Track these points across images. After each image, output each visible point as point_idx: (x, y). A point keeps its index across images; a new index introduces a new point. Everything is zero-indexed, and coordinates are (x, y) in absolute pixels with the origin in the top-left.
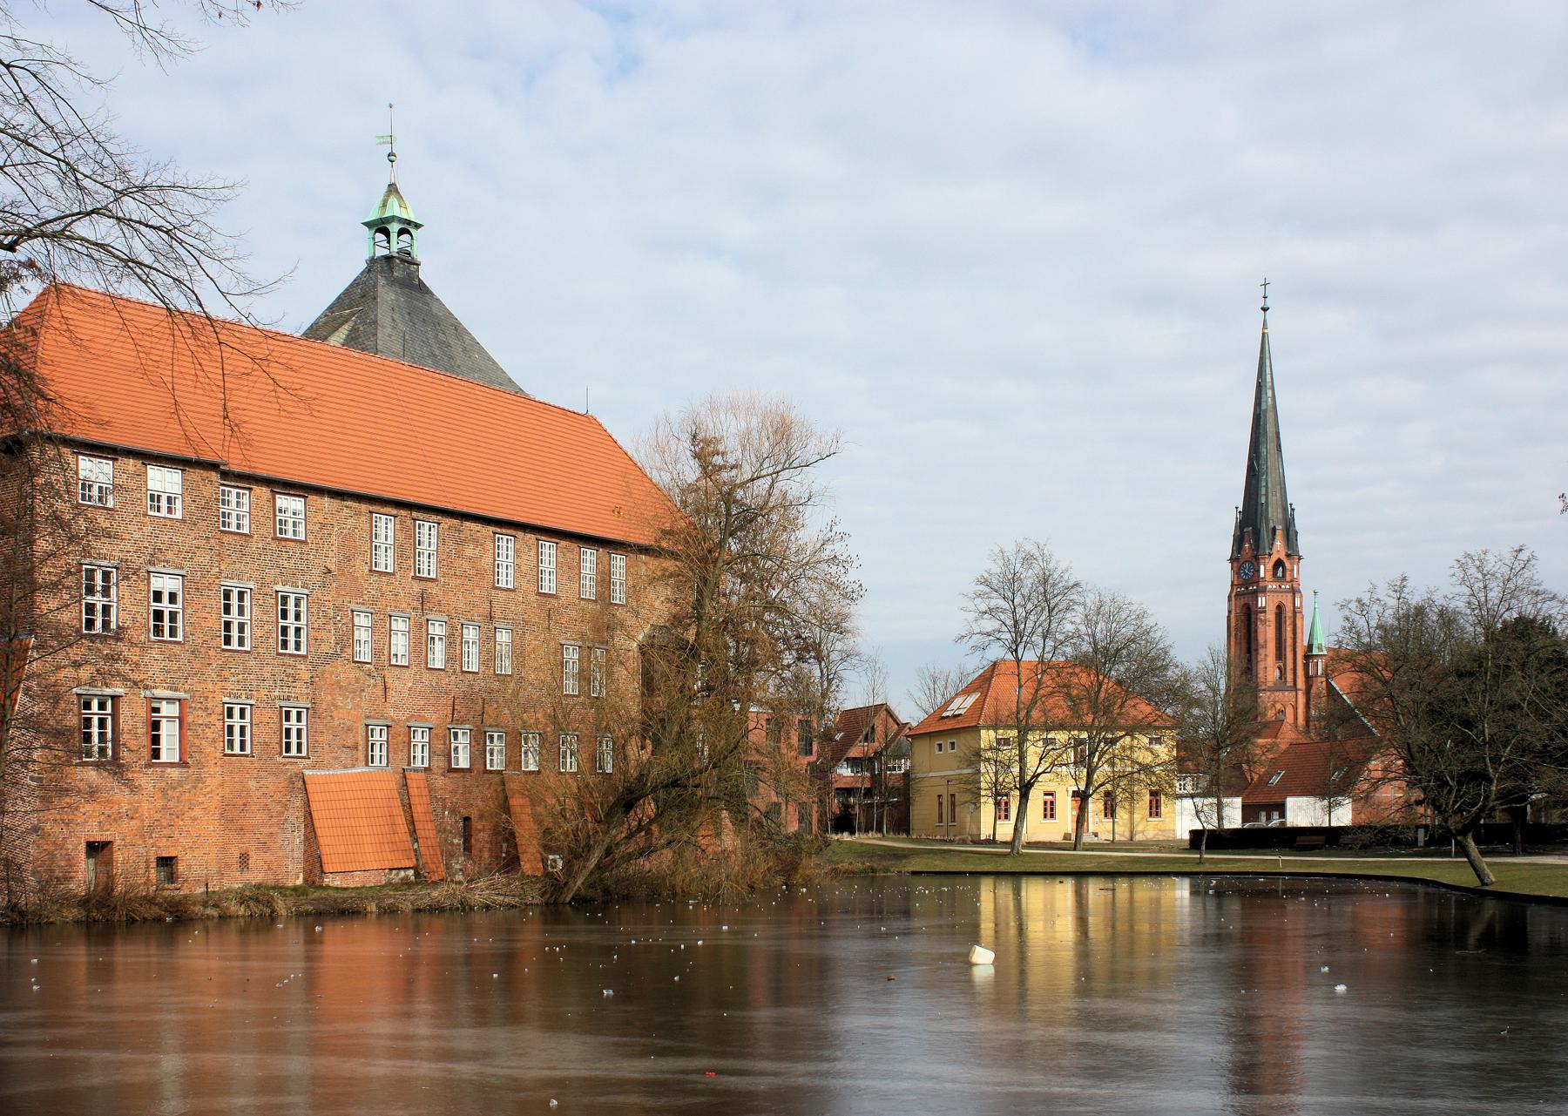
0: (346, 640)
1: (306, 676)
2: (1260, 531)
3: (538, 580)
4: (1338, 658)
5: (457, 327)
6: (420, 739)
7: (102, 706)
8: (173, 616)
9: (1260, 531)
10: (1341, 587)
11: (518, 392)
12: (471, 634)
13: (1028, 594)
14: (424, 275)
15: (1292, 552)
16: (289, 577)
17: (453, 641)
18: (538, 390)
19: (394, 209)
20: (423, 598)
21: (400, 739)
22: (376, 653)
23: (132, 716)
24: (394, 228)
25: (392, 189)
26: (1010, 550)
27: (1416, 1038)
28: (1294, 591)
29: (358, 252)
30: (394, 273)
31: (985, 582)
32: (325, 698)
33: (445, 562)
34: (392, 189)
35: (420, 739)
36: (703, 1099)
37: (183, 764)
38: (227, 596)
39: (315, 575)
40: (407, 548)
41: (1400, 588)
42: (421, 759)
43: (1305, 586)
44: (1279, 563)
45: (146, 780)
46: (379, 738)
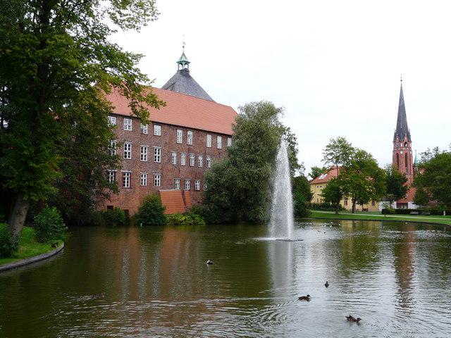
0: (170, 159)
1: (160, 167)
2: (402, 134)
3: (216, 145)
4: (421, 166)
5: (198, 86)
6: (188, 183)
7: (128, 175)
8: (129, 153)
9: (402, 134)
10: (423, 146)
11: (215, 102)
12: (200, 158)
13: (341, 148)
14: (190, 74)
15: (409, 141)
16: (157, 145)
17: (196, 159)
18: (218, 101)
19: (184, 59)
20: (189, 149)
21: (183, 184)
22: (177, 162)
23: (119, 177)
24: (184, 63)
25: (184, 54)
26: (336, 140)
27: (430, 292)
28: (410, 150)
29: (173, 70)
30: (185, 73)
31: (328, 146)
32: (165, 173)
33: (194, 141)
34: (184, 54)
35: (188, 183)
36: (289, 262)
37: (131, 188)
38: (142, 148)
39: (163, 144)
40: (185, 137)
41: (437, 150)
42: (188, 188)
43: (413, 149)
44: (406, 143)
45: (122, 192)
46: (178, 182)
